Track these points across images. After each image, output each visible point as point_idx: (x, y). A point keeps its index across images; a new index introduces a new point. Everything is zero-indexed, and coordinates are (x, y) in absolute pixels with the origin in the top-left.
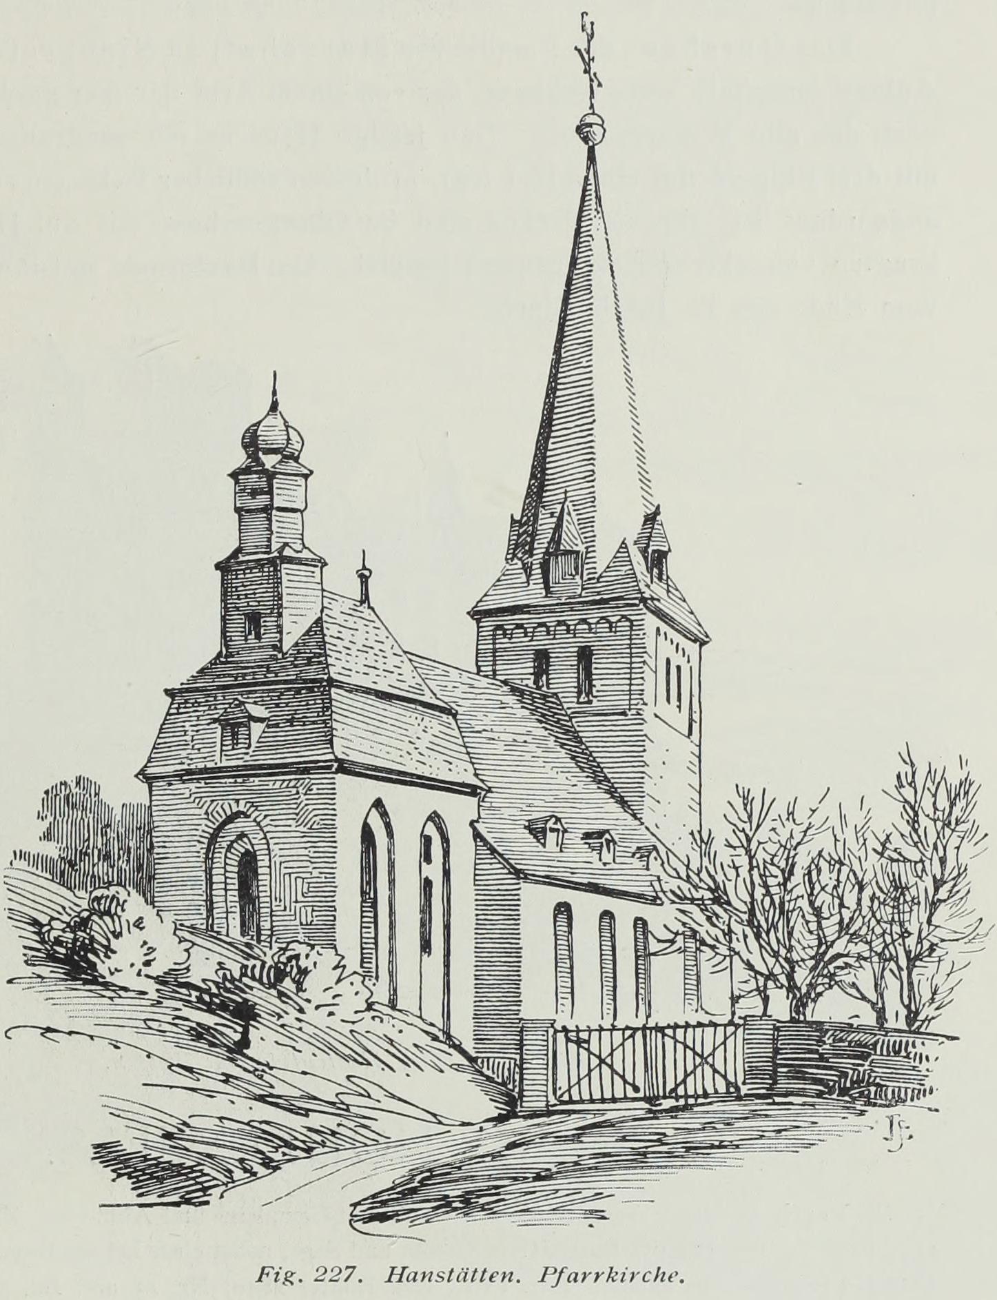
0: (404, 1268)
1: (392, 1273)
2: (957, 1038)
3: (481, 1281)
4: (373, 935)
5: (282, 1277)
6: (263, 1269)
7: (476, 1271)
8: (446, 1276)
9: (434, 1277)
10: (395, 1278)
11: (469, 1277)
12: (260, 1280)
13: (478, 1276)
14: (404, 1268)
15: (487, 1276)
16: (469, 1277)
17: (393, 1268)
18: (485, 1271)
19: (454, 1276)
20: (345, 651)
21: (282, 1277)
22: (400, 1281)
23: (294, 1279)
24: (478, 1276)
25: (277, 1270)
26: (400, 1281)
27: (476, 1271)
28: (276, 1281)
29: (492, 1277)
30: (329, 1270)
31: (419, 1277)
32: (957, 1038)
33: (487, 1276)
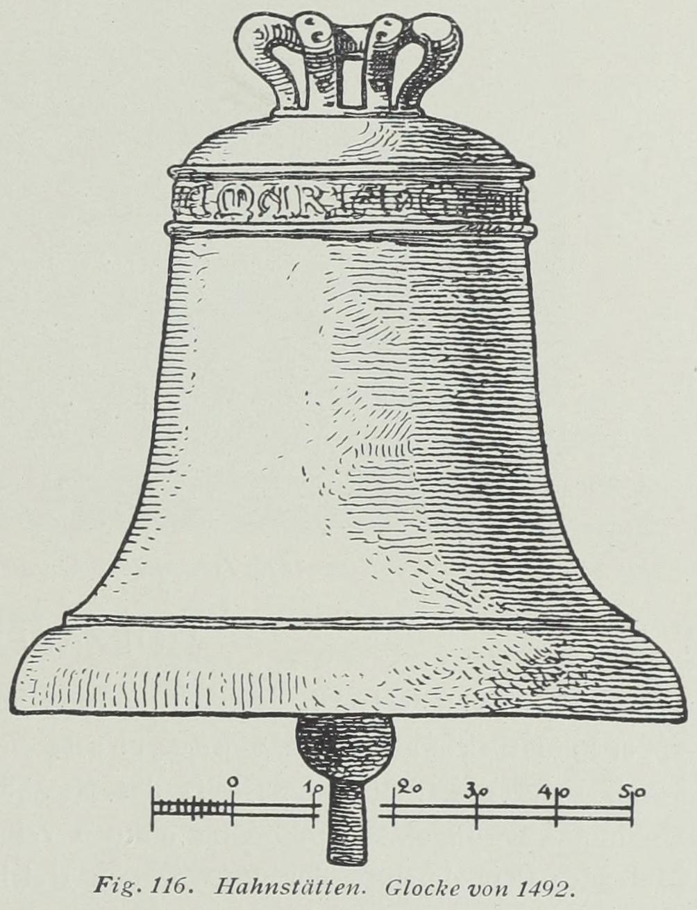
0: (234, 880)
1: (221, 885)
2: (152, 829)
3: (317, 893)
4: (531, 373)
5: (120, 888)
6: (102, 878)
7: (321, 883)
8: (291, 888)
9: (279, 889)
10: (225, 889)
11: (314, 889)
12: (98, 890)
13: (323, 888)
14: (234, 880)
15: (333, 888)
16: (314, 889)
17: (223, 880)
18: (331, 883)
19: (299, 888)
20: (112, 681)
21: (120, 888)
22: (230, 892)
23: (133, 889)
24: (323, 888)
25: (115, 880)
26: (230, 892)
27: (321, 883)
28: (114, 891)
29: (337, 889)
30: (555, 885)
31: (264, 888)
32: (152, 829)
33: (333, 888)
